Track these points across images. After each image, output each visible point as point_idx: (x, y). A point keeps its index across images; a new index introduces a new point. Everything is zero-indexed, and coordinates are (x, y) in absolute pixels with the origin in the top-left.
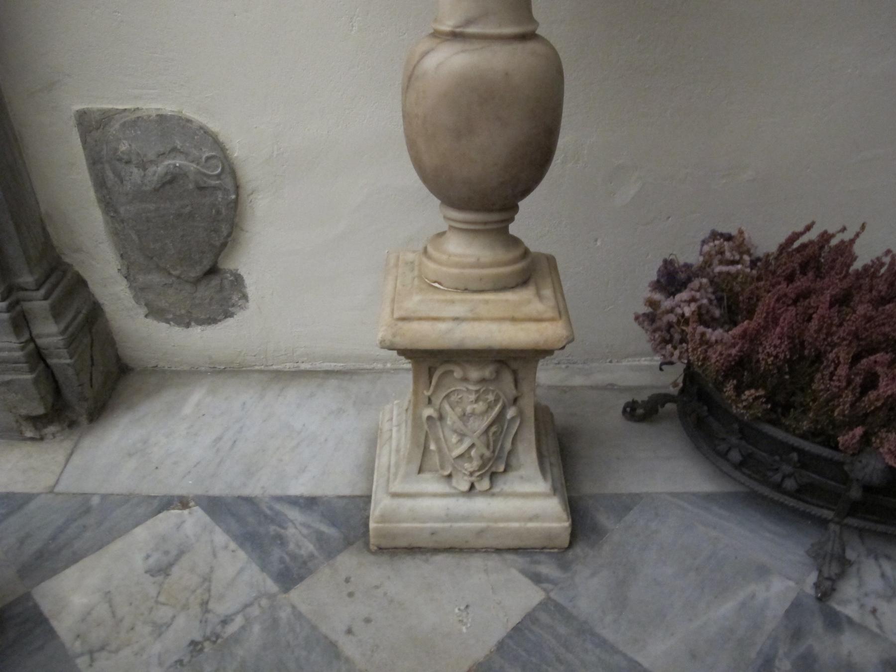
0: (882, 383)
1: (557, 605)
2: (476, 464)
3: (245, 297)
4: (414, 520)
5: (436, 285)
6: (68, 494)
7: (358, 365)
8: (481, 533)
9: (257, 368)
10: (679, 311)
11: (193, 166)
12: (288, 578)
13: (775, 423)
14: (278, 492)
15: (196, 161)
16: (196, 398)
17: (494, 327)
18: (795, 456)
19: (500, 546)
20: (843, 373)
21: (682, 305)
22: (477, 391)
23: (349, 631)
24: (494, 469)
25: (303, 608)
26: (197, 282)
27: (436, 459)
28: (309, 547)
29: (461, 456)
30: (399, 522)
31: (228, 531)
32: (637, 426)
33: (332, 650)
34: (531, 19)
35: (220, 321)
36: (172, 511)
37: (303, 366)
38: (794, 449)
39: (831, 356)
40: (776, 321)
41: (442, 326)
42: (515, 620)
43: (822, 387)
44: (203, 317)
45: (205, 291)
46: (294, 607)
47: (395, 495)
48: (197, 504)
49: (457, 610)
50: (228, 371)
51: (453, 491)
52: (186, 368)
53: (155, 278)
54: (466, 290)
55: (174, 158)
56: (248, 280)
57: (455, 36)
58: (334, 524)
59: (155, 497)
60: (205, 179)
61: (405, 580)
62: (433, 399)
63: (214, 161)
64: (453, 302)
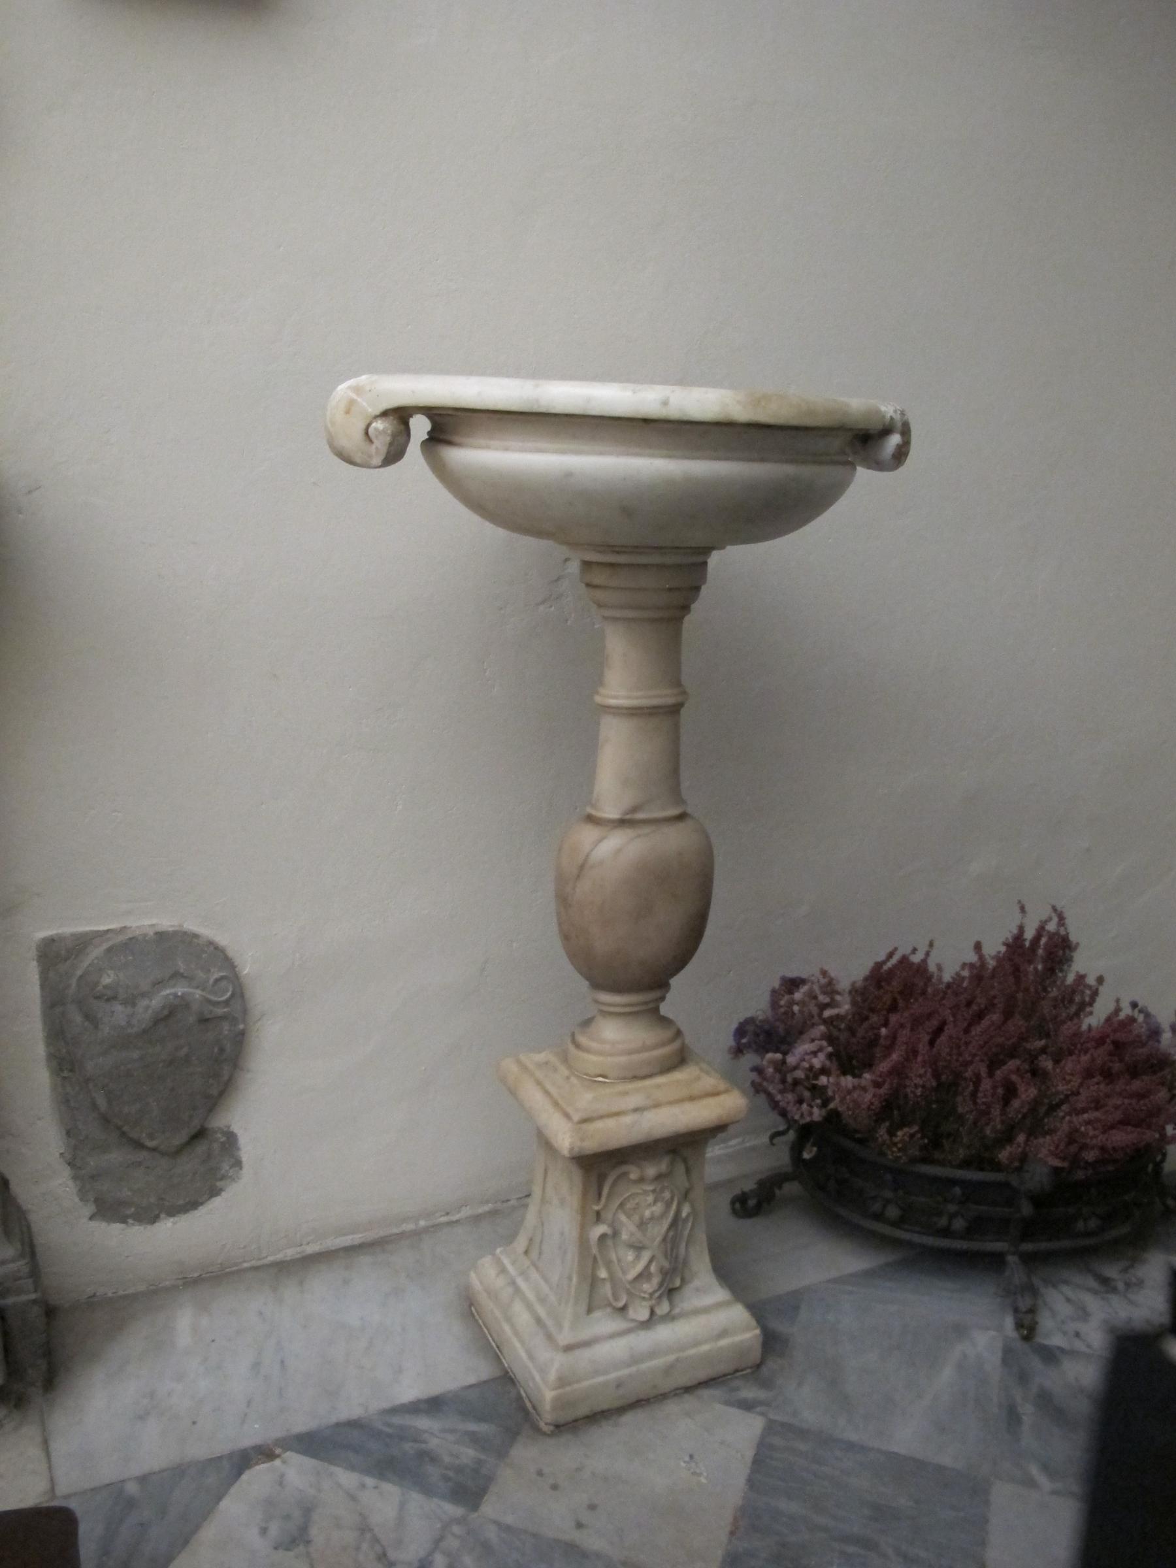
0: (1021, 1088)
1: (783, 1425)
2: (656, 1281)
3: (238, 1164)
4: (597, 1373)
5: (601, 1079)
6: (84, 1492)
7: (382, 1233)
8: (668, 1370)
9: (246, 1265)
10: (806, 1065)
11: (198, 993)
12: (469, 1490)
13: (932, 1162)
14: (386, 1405)
15: (202, 986)
16: (184, 1322)
17: (675, 1110)
18: (957, 1190)
19: (689, 1384)
20: (988, 1087)
21: (807, 1057)
22: (654, 1191)
23: (579, 1526)
24: (671, 1286)
25: (509, 1519)
26: (179, 1151)
27: (607, 1290)
28: (468, 1454)
29: (640, 1277)
30: (578, 1381)
31: (352, 1468)
32: (748, 1222)
33: (572, 1550)
34: (683, 802)
35: (202, 1204)
36: (257, 1467)
37: (310, 1249)
38: (953, 1182)
39: (969, 1074)
40: (915, 1053)
41: (627, 1119)
42: (749, 1454)
43: (967, 1109)
44: (181, 1202)
45: (187, 1165)
46: (495, 1522)
47: (569, 1348)
48: (286, 1450)
49: (683, 1464)
50: (208, 1279)
51: (632, 1325)
52: (142, 1288)
53: (116, 1157)
54: (635, 1078)
55: (174, 986)
56: (243, 1141)
57: (622, 823)
58: (481, 1419)
59: (220, 1458)
60: (211, 1008)
61: (606, 1452)
62: (603, 1214)
63: (224, 983)
64: (626, 1093)
